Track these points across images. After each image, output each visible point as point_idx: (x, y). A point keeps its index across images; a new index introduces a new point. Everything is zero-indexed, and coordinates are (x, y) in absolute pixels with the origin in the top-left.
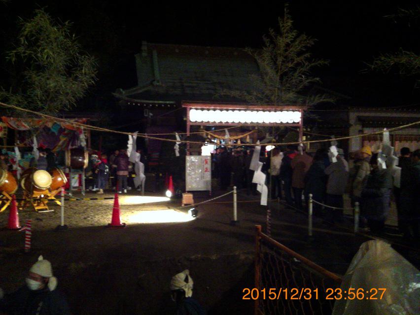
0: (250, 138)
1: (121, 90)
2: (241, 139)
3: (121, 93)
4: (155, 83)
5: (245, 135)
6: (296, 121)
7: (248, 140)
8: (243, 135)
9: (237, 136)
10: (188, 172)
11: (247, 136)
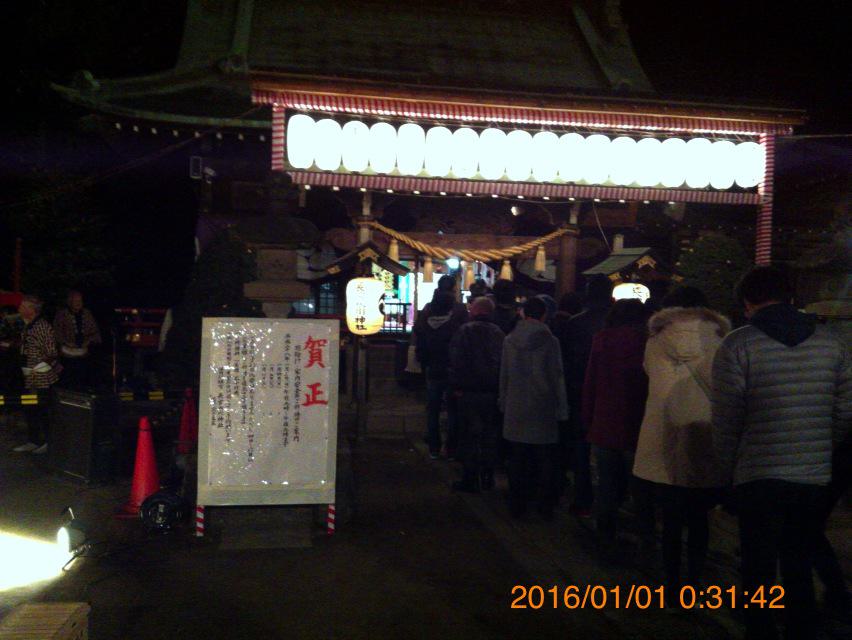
0: (548, 257)
1: (89, 76)
2: (514, 261)
3: (84, 85)
4: (229, 67)
5: (529, 245)
6: (745, 184)
7: (541, 264)
8: (520, 244)
9: (500, 247)
10: (208, 402)
11: (536, 248)
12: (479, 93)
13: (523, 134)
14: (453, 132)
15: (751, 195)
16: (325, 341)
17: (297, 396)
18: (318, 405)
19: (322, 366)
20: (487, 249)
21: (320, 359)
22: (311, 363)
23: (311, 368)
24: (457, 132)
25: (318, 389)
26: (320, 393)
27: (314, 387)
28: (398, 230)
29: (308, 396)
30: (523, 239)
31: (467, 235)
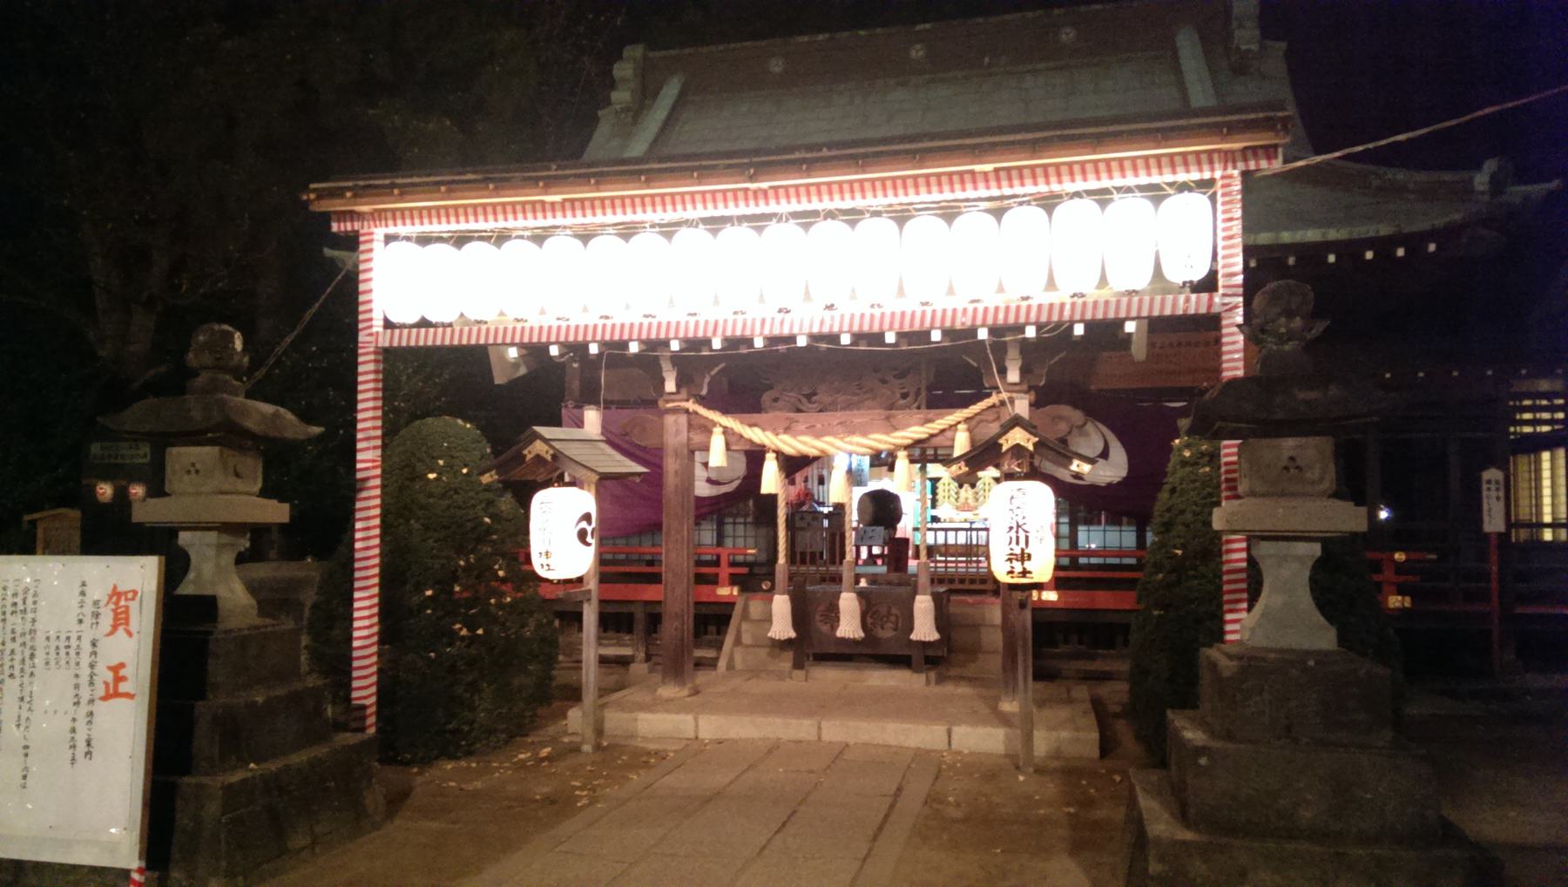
11: (953, 427)
12: (804, 161)
13: (837, 227)
14: (627, 242)
15: (1205, 296)
16: (135, 593)
17: (91, 683)
18: (123, 700)
19: (130, 634)
20: (864, 434)
21: (127, 622)
22: (115, 627)
23: (112, 637)
24: (958, 221)
25: (122, 672)
26: (123, 679)
27: (116, 669)
28: (725, 411)
29: (107, 684)
30: (932, 413)
31: (839, 414)
